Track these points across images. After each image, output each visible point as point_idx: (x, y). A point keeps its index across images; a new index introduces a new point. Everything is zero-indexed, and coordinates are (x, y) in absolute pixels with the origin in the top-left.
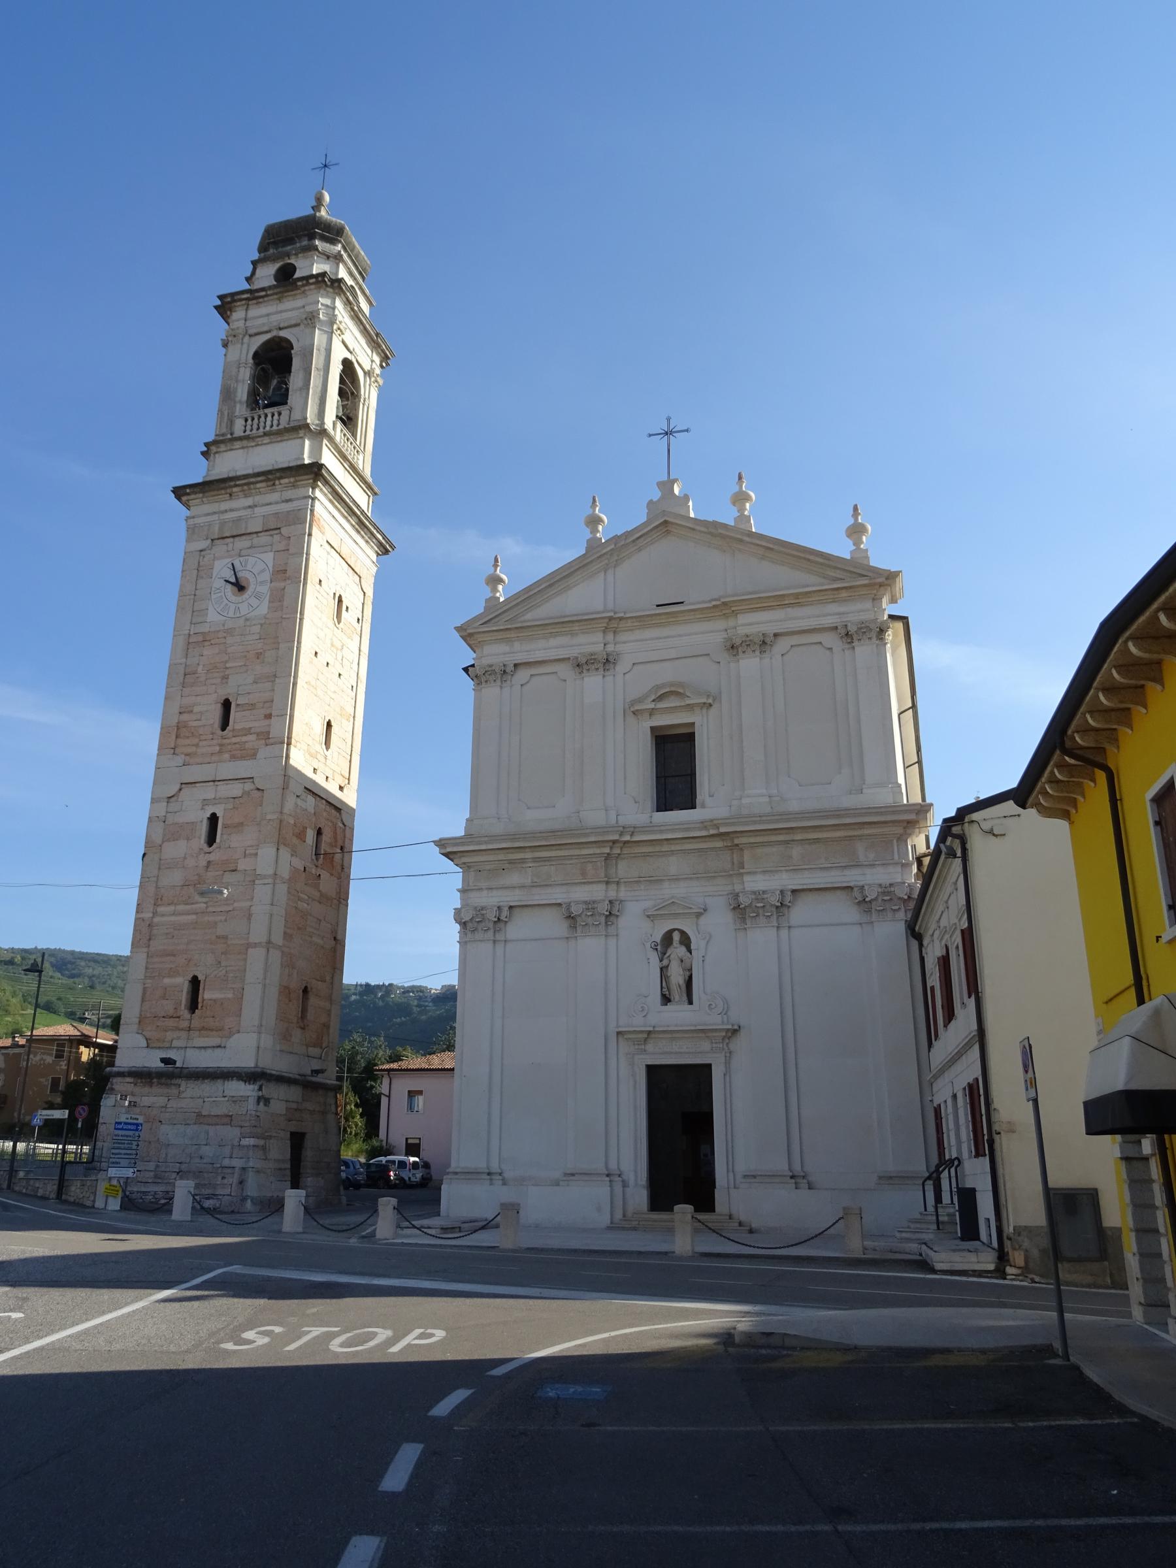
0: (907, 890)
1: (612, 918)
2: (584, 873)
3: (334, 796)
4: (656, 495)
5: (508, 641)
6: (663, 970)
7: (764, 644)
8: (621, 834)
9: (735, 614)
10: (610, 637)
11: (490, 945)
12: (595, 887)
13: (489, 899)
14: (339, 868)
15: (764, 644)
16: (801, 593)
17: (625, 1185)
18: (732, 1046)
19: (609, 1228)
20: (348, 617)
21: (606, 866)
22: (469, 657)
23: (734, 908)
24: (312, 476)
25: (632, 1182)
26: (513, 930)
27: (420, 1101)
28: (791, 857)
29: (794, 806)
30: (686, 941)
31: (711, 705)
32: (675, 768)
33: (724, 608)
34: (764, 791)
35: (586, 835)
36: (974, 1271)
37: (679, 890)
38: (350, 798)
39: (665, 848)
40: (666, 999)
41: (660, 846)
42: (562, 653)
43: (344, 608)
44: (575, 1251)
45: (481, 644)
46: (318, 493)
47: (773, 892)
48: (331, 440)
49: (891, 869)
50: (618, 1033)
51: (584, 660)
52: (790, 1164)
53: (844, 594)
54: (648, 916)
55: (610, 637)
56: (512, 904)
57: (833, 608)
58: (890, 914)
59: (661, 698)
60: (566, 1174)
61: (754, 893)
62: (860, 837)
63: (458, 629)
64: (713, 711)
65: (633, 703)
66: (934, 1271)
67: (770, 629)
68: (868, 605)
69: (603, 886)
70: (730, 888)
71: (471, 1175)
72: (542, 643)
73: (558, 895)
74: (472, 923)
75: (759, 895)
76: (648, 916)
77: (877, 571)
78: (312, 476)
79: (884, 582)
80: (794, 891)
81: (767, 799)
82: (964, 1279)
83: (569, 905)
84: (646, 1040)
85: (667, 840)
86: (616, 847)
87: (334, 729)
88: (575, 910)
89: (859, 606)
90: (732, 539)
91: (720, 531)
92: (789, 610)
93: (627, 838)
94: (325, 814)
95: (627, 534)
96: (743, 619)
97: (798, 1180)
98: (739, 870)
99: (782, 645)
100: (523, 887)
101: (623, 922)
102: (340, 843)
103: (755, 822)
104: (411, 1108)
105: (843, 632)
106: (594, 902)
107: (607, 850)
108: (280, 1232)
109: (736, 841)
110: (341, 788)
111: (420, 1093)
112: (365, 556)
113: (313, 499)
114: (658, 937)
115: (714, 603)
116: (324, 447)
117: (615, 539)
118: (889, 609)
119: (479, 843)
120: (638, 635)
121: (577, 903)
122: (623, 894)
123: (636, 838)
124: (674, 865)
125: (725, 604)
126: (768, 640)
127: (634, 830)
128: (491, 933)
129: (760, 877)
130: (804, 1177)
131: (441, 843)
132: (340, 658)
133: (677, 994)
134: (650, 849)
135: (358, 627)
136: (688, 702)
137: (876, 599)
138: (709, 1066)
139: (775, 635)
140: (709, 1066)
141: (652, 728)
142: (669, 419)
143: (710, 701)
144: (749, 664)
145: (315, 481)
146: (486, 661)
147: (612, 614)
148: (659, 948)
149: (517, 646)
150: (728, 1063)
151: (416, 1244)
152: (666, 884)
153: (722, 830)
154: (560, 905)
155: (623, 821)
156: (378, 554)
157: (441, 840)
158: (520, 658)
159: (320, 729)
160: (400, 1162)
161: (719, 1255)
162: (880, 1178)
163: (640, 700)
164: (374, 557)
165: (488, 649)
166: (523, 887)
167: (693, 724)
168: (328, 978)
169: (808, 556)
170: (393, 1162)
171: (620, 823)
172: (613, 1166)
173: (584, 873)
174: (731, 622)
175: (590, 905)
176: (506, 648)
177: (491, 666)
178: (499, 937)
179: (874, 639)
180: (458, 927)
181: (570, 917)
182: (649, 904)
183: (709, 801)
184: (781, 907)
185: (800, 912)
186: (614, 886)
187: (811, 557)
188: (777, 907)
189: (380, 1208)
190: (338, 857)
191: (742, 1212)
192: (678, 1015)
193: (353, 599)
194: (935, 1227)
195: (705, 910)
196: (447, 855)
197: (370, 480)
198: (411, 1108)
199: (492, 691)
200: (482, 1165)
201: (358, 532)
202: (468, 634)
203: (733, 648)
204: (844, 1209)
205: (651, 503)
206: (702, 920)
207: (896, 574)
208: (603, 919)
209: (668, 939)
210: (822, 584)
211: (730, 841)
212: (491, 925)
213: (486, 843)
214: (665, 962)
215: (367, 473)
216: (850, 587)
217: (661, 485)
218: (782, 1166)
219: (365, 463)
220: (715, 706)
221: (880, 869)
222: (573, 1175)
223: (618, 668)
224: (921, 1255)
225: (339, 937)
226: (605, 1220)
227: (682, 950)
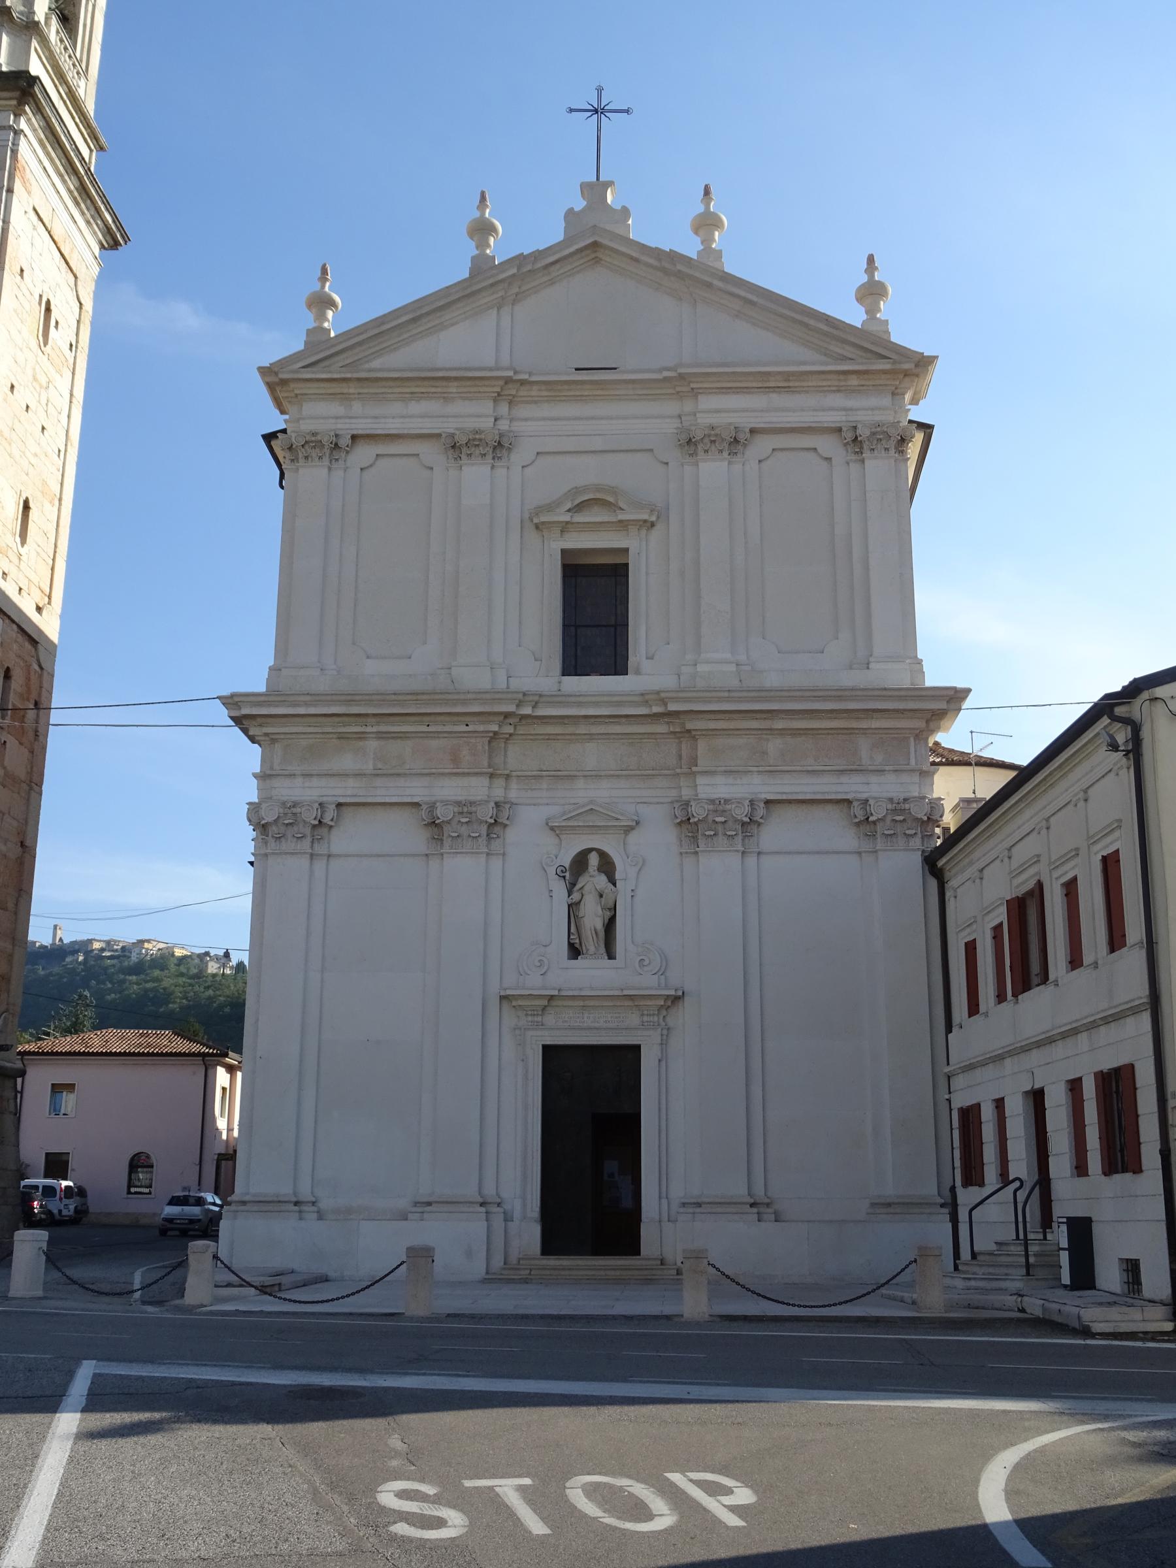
0: (927, 809)
1: (497, 829)
2: (456, 760)
3: (30, 620)
4: (579, 204)
5: (345, 398)
6: (573, 908)
7: (735, 443)
8: (519, 705)
9: (695, 393)
10: (504, 409)
11: (305, 861)
12: (474, 781)
13: (306, 791)
14: (31, 734)
15: (735, 443)
16: (793, 374)
17: (508, 1218)
18: (671, 1021)
19: (484, 1281)
20: (61, 337)
21: (491, 752)
22: (276, 421)
23: (680, 824)
24: (17, 94)
25: (517, 1214)
26: (339, 841)
27: (69, 1101)
28: (765, 753)
29: (772, 680)
30: (607, 867)
31: (653, 525)
32: (594, 611)
33: (682, 383)
34: (728, 656)
35: (464, 702)
36: (1145, 1333)
37: (601, 792)
38: (50, 625)
39: (582, 729)
40: (575, 951)
41: (575, 725)
42: (428, 427)
43: (53, 323)
44: (525, 1318)
45: (299, 399)
46: (23, 125)
47: (739, 802)
48: (44, 41)
49: (905, 778)
50: (503, 998)
51: (464, 440)
52: (749, 1188)
53: (854, 381)
54: (552, 829)
55: (504, 409)
56: (342, 800)
57: (837, 400)
58: (901, 841)
59: (579, 507)
60: (416, 1204)
61: (712, 801)
62: (864, 732)
63: (263, 371)
64: (656, 534)
65: (539, 510)
66: (1093, 1336)
67: (747, 421)
68: (886, 401)
69: (485, 781)
70: (674, 793)
71: (269, 1205)
72: (397, 408)
73: (415, 790)
74: (274, 827)
75: (719, 805)
76: (552, 829)
77: (903, 353)
78: (17, 94)
79: (913, 368)
80: (768, 802)
81: (733, 668)
82: (1139, 1344)
83: (432, 807)
84: (544, 1008)
85: (586, 717)
86: (506, 723)
87: (33, 514)
88: (443, 813)
89: (873, 401)
90: (694, 280)
91: (679, 267)
92: (774, 396)
93: (527, 711)
94: (15, 646)
95: (537, 255)
96: (707, 402)
97: (305, 1208)
98: (690, 769)
99: (762, 445)
100: (359, 775)
101: (512, 835)
102: (34, 696)
103: (720, 700)
104: (55, 1109)
105: (849, 436)
106: (472, 803)
107: (495, 728)
108: (6, 1298)
109: (689, 726)
110: (39, 609)
111: (70, 1087)
112: (84, 243)
113: (18, 133)
114: (566, 860)
115: (666, 374)
116: (33, 55)
117: (520, 259)
118: (917, 413)
119: (295, 705)
120: (546, 410)
121: (446, 803)
122: (513, 795)
123: (540, 712)
124: (591, 755)
125: (681, 377)
126: (741, 437)
127: (539, 699)
128: (307, 843)
129: (720, 779)
130: (499, 1205)
131: (231, 701)
132: (44, 402)
133: (592, 944)
134: (558, 730)
135: (70, 356)
136: (621, 517)
137: (896, 394)
138: (636, 1049)
139: (753, 431)
140: (636, 1049)
141: (564, 552)
142: (600, 90)
143: (653, 518)
144: (713, 470)
145: (21, 102)
146: (307, 426)
147: (510, 373)
148: (567, 875)
149: (357, 407)
150: (664, 1044)
151: (237, 1313)
152: (580, 783)
153: (672, 707)
154: (417, 805)
155: (515, 684)
156: (102, 247)
157: (233, 696)
158: (362, 426)
159: (13, 510)
160: (45, 1187)
161: (746, 1319)
162: (873, 1205)
163: (550, 508)
164: (96, 249)
165: (309, 408)
166: (359, 775)
167: (626, 550)
168: (11, 905)
169: (806, 320)
170: (36, 1187)
171: (512, 688)
172: (490, 1191)
173: (456, 760)
174: (688, 406)
175: (466, 808)
176: (336, 408)
177: (314, 434)
178: (320, 849)
179: (892, 451)
180: (249, 832)
181: (434, 824)
182: (554, 810)
183: (646, 665)
184: (749, 825)
185: (777, 832)
186: (500, 782)
187: (812, 322)
188: (743, 824)
189: (191, 1258)
190: (31, 714)
191: (674, 1251)
192: (592, 973)
193: (65, 311)
194: (1024, 1271)
195: (638, 823)
196: (238, 721)
197: (94, 124)
198: (55, 1109)
199: (312, 475)
200: (285, 1190)
201: (77, 204)
202: (279, 382)
203: (690, 444)
204: (920, 1248)
205: (570, 213)
206: (633, 838)
207: (931, 360)
208: (484, 829)
209: (580, 863)
210: (827, 364)
211: (678, 724)
212: (308, 831)
213: (306, 704)
214: (576, 896)
215: (90, 107)
216: (866, 372)
217: (586, 188)
218: (739, 1191)
219: (87, 91)
220: (659, 527)
221: (891, 778)
222: (429, 1204)
223: (514, 457)
224: (1023, 1310)
225: (28, 843)
226: (478, 1268)
227: (601, 881)
